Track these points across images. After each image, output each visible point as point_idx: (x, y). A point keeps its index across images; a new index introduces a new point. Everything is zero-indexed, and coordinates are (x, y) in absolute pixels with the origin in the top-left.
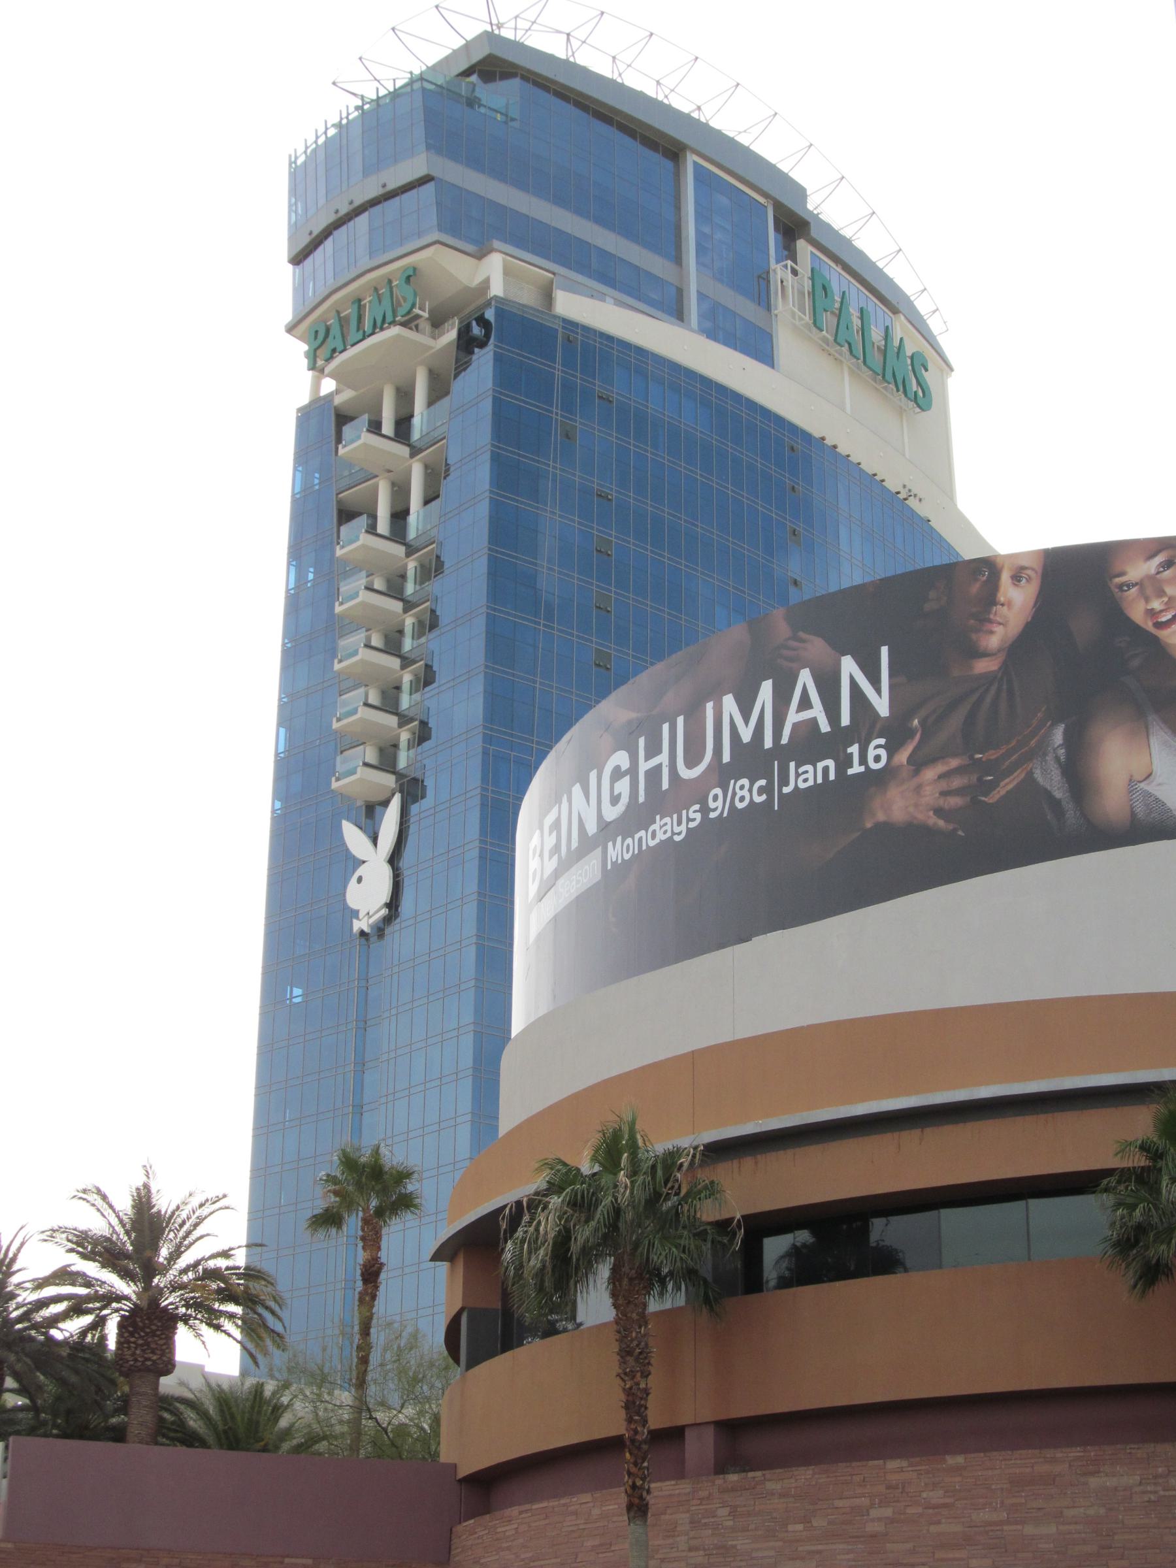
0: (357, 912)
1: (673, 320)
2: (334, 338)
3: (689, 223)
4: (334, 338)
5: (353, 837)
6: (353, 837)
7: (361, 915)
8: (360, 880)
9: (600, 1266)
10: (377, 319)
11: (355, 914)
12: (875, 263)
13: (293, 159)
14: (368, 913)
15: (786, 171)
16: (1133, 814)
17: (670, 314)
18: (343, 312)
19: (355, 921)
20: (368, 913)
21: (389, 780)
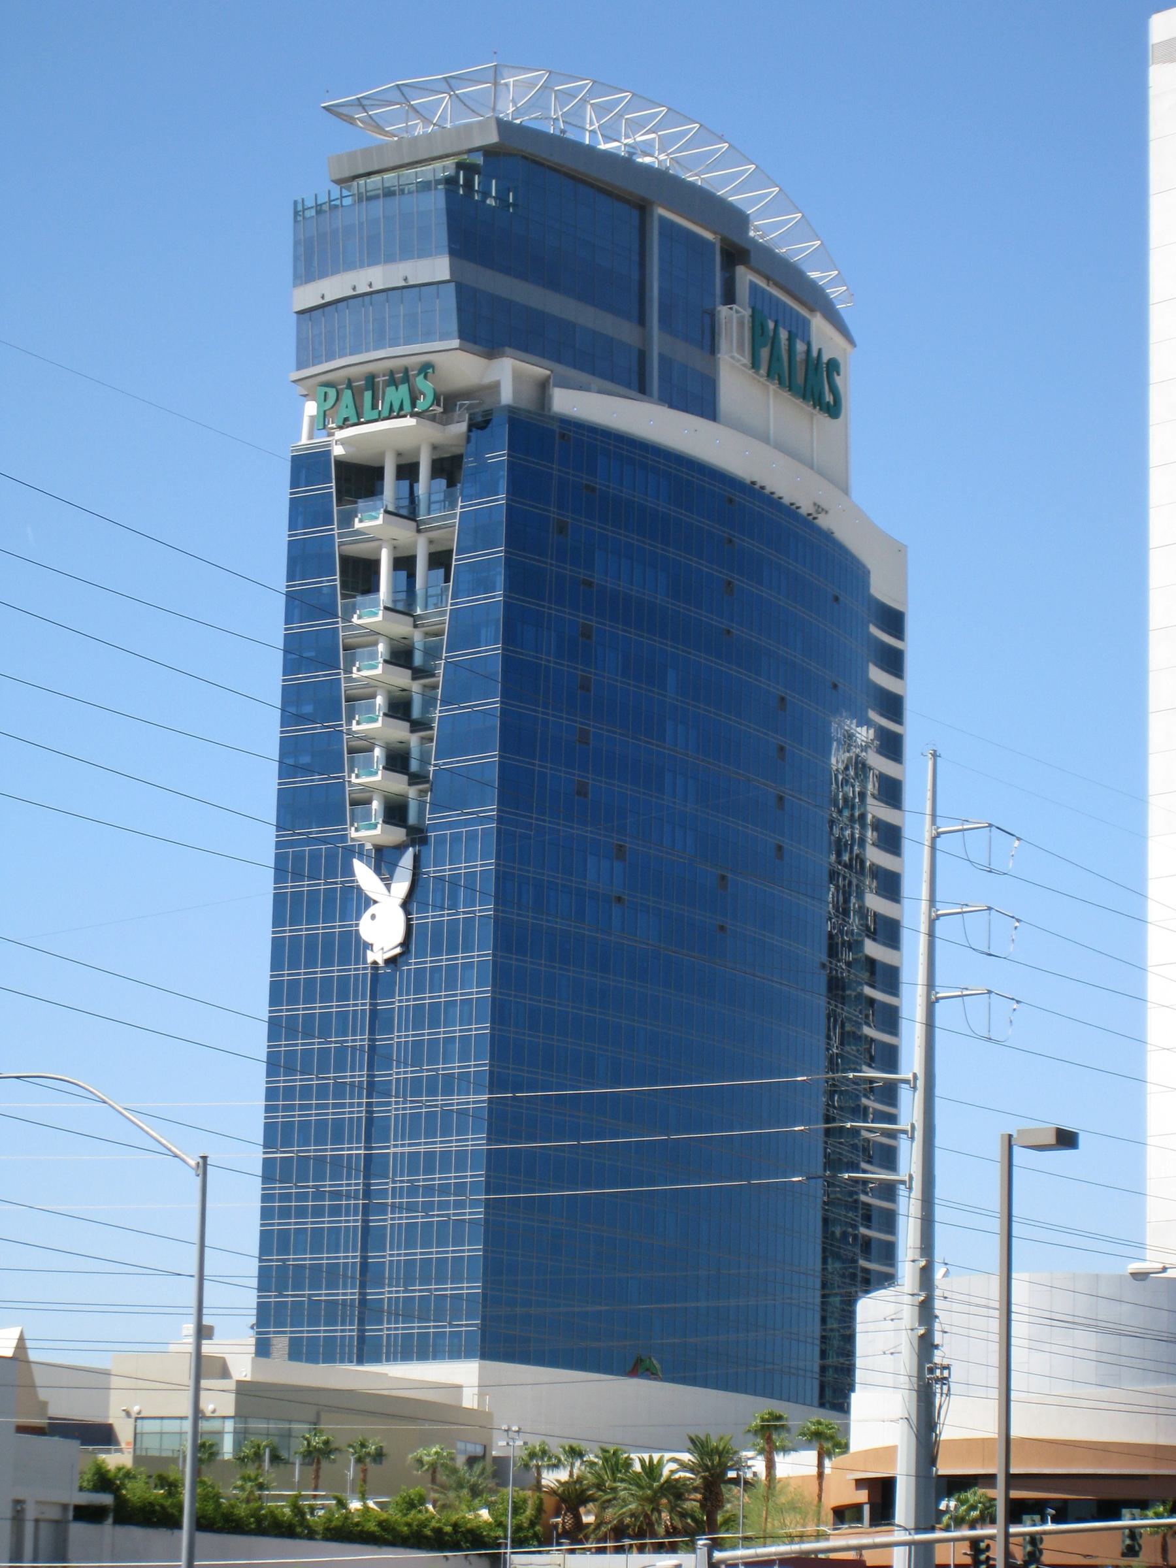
0: (372, 945)
1: (634, 394)
2: (347, 407)
3: (892, 1003)
4: (347, 407)
5: (364, 875)
6: (364, 875)
7: (375, 948)
8: (373, 917)
9: (99, 1458)
10: (393, 403)
11: (369, 946)
12: (935, 1027)
13: (300, 208)
14: (382, 949)
15: (936, 1094)
16: (784, 1455)
17: (628, 386)
18: (354, 382)
19: (369, 952)
20: (382, 949)
21: (397, 835)
